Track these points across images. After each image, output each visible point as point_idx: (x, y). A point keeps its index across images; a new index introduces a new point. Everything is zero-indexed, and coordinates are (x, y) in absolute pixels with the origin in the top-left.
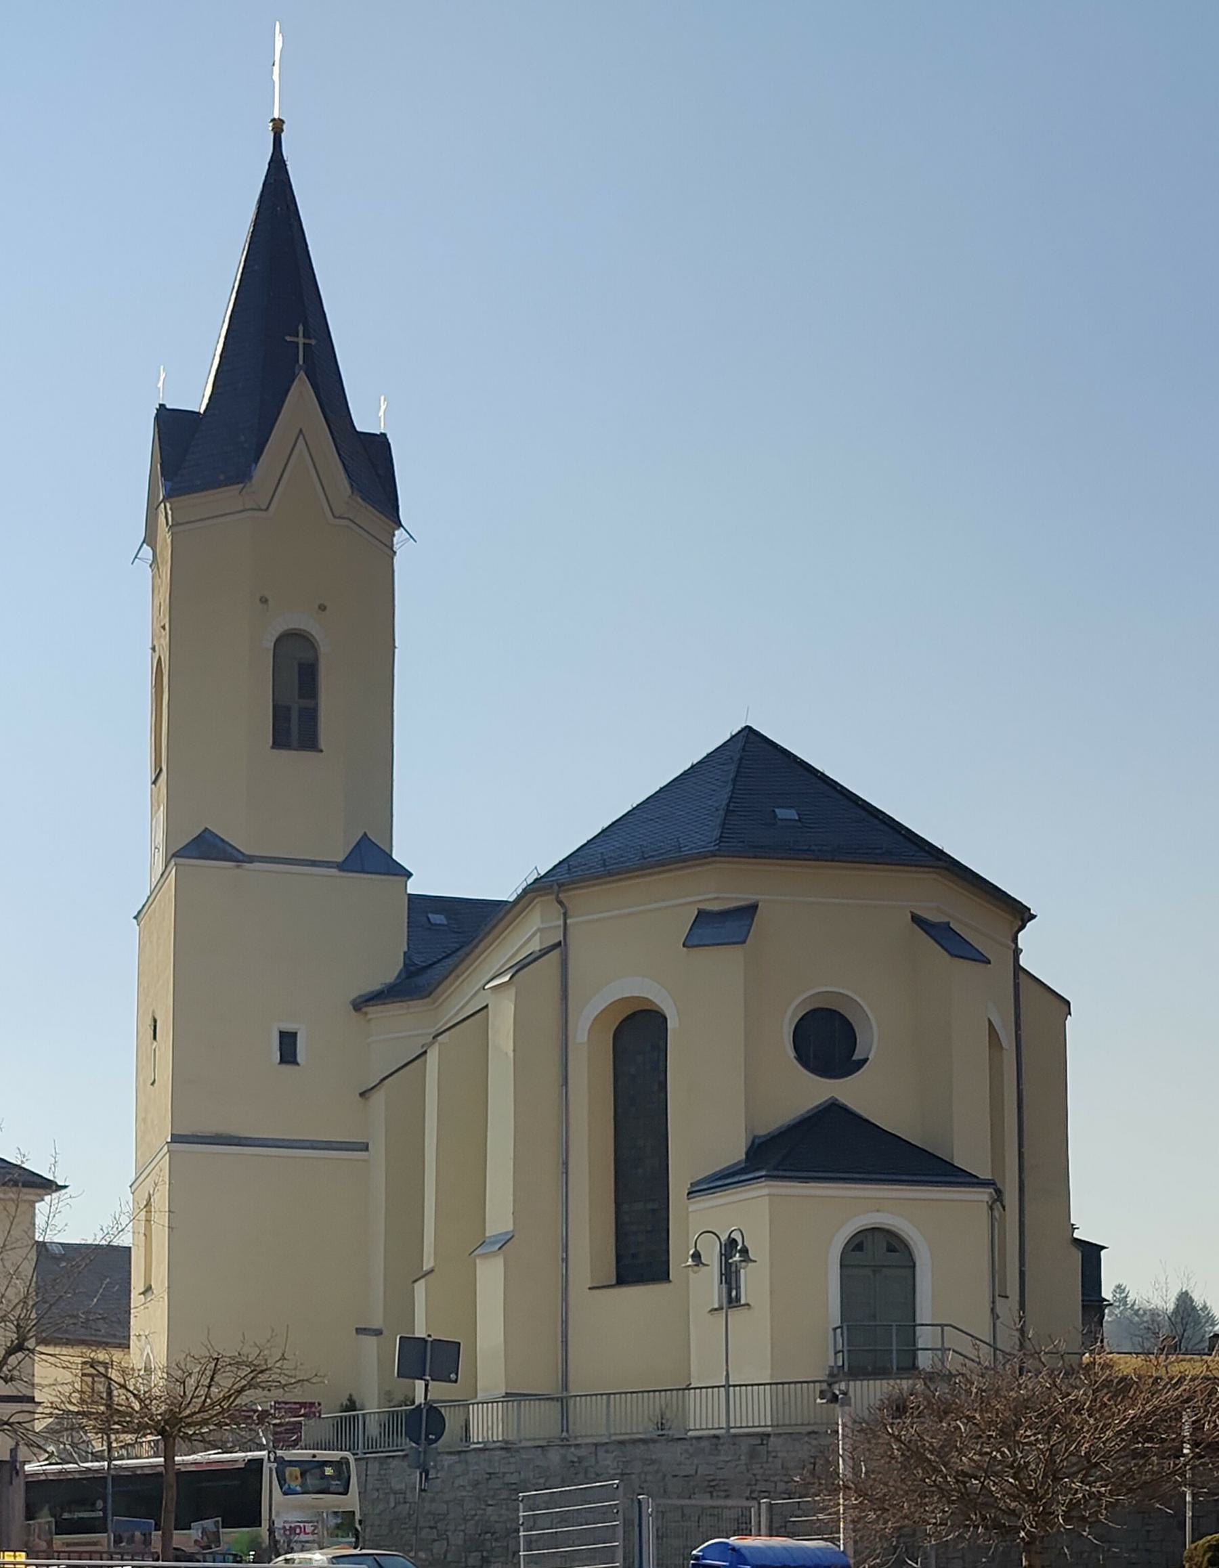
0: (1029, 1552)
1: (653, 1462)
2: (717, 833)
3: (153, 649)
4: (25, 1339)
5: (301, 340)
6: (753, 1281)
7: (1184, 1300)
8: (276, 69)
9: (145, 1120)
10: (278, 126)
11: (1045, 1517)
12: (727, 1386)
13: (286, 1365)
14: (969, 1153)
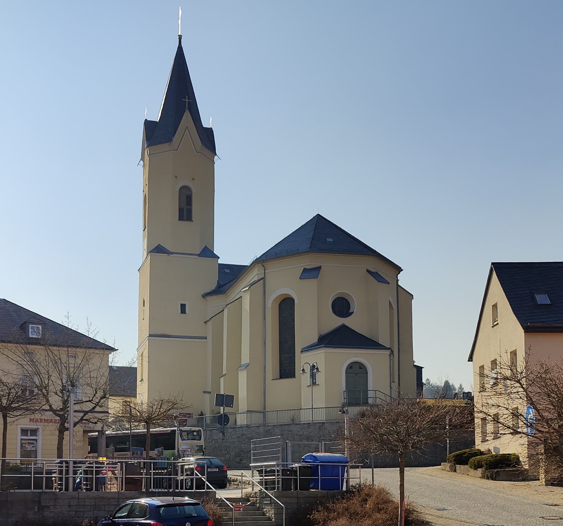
0: (401, 457)
1: (290, 431)
2: (309, 246)
5: (187, 100)
6: (320, 377)
7: (447, 383)
8: (180, 20)
9: (141, 330)
10: (180, 37)
11: (406, 447)
13: (183, 402)
14: (383, 340)
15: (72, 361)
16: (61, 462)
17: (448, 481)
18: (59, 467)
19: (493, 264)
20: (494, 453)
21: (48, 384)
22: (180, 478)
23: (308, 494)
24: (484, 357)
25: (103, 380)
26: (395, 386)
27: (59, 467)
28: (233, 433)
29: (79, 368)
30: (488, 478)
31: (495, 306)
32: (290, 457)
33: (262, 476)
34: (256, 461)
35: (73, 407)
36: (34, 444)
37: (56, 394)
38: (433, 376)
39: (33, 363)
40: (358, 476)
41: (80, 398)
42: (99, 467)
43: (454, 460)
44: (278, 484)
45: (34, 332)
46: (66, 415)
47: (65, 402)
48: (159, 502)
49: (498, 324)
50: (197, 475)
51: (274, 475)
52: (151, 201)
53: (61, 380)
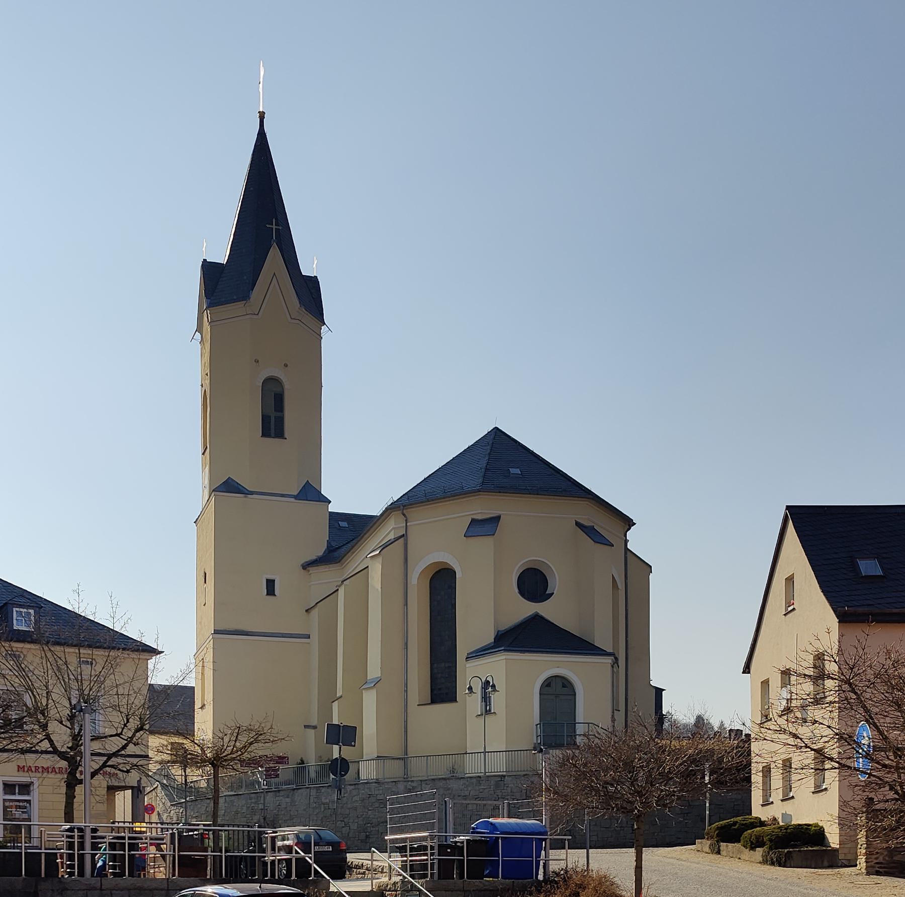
0: (637, 822)
1: (449, 789)
2: (481, 480)
3: (202, 386)
4: (144, 725)
5: (274, 227)
6: (498, 701)
7: (699, 719)
8: (261, 85)
10: (262, 116)
11: (646, 804)
12: (485, 752)
14: (602, 640)
15: (87, 669)
16: (71, 830)
17: (708, 868)
18: (68, 837)
19: (788, 508)
20: (781, 824)
21: (47, 705)
22: (269, 858)
23: (482, 885)
24: (768, 665)
25: (139, 701)
26: (620, 716)
27: (68, 837)
28: (354, 792)
29: (99, 680)
30: (773, 864)
31: (790, 580)
32: (450, 826)
33: (406, 856)
34: (392, 834)
35: (89, 746)
36: (25, 808)
37: (61, 722)
38: (680, 708)
39: (22, 671)
40: (562, 860)
41: (101, 730)
42: (135, 838)
43: (718, 835)
44: (432, 869)
45: (21, 621)
46: (79, 758)
47: (76, 738)
48: (235, 891)
49: (794, 609)
50: (297, 852)
51: (426, 855)
52: (215, 402)
53: (69, 699)
